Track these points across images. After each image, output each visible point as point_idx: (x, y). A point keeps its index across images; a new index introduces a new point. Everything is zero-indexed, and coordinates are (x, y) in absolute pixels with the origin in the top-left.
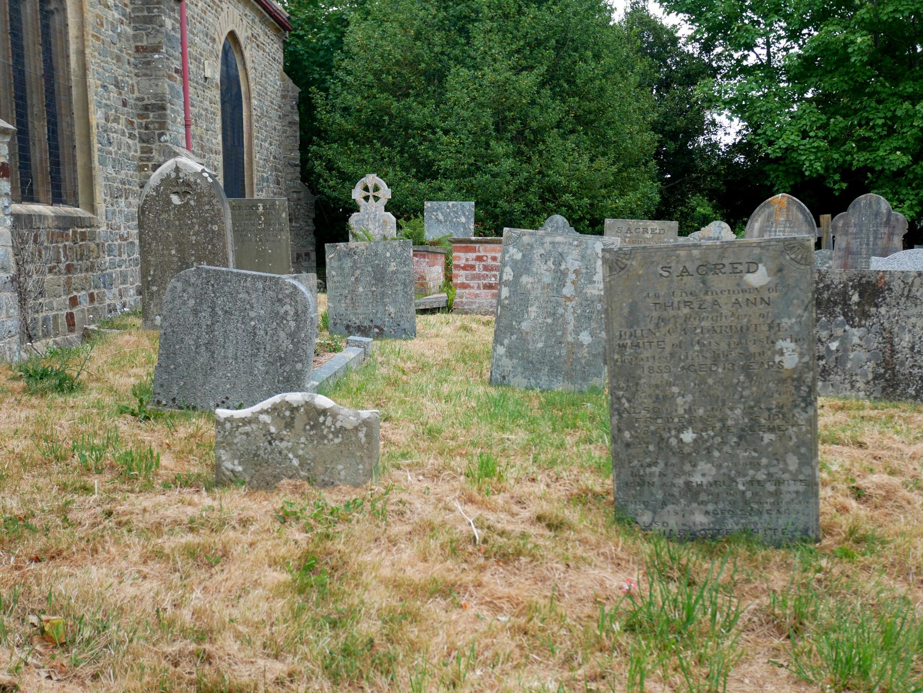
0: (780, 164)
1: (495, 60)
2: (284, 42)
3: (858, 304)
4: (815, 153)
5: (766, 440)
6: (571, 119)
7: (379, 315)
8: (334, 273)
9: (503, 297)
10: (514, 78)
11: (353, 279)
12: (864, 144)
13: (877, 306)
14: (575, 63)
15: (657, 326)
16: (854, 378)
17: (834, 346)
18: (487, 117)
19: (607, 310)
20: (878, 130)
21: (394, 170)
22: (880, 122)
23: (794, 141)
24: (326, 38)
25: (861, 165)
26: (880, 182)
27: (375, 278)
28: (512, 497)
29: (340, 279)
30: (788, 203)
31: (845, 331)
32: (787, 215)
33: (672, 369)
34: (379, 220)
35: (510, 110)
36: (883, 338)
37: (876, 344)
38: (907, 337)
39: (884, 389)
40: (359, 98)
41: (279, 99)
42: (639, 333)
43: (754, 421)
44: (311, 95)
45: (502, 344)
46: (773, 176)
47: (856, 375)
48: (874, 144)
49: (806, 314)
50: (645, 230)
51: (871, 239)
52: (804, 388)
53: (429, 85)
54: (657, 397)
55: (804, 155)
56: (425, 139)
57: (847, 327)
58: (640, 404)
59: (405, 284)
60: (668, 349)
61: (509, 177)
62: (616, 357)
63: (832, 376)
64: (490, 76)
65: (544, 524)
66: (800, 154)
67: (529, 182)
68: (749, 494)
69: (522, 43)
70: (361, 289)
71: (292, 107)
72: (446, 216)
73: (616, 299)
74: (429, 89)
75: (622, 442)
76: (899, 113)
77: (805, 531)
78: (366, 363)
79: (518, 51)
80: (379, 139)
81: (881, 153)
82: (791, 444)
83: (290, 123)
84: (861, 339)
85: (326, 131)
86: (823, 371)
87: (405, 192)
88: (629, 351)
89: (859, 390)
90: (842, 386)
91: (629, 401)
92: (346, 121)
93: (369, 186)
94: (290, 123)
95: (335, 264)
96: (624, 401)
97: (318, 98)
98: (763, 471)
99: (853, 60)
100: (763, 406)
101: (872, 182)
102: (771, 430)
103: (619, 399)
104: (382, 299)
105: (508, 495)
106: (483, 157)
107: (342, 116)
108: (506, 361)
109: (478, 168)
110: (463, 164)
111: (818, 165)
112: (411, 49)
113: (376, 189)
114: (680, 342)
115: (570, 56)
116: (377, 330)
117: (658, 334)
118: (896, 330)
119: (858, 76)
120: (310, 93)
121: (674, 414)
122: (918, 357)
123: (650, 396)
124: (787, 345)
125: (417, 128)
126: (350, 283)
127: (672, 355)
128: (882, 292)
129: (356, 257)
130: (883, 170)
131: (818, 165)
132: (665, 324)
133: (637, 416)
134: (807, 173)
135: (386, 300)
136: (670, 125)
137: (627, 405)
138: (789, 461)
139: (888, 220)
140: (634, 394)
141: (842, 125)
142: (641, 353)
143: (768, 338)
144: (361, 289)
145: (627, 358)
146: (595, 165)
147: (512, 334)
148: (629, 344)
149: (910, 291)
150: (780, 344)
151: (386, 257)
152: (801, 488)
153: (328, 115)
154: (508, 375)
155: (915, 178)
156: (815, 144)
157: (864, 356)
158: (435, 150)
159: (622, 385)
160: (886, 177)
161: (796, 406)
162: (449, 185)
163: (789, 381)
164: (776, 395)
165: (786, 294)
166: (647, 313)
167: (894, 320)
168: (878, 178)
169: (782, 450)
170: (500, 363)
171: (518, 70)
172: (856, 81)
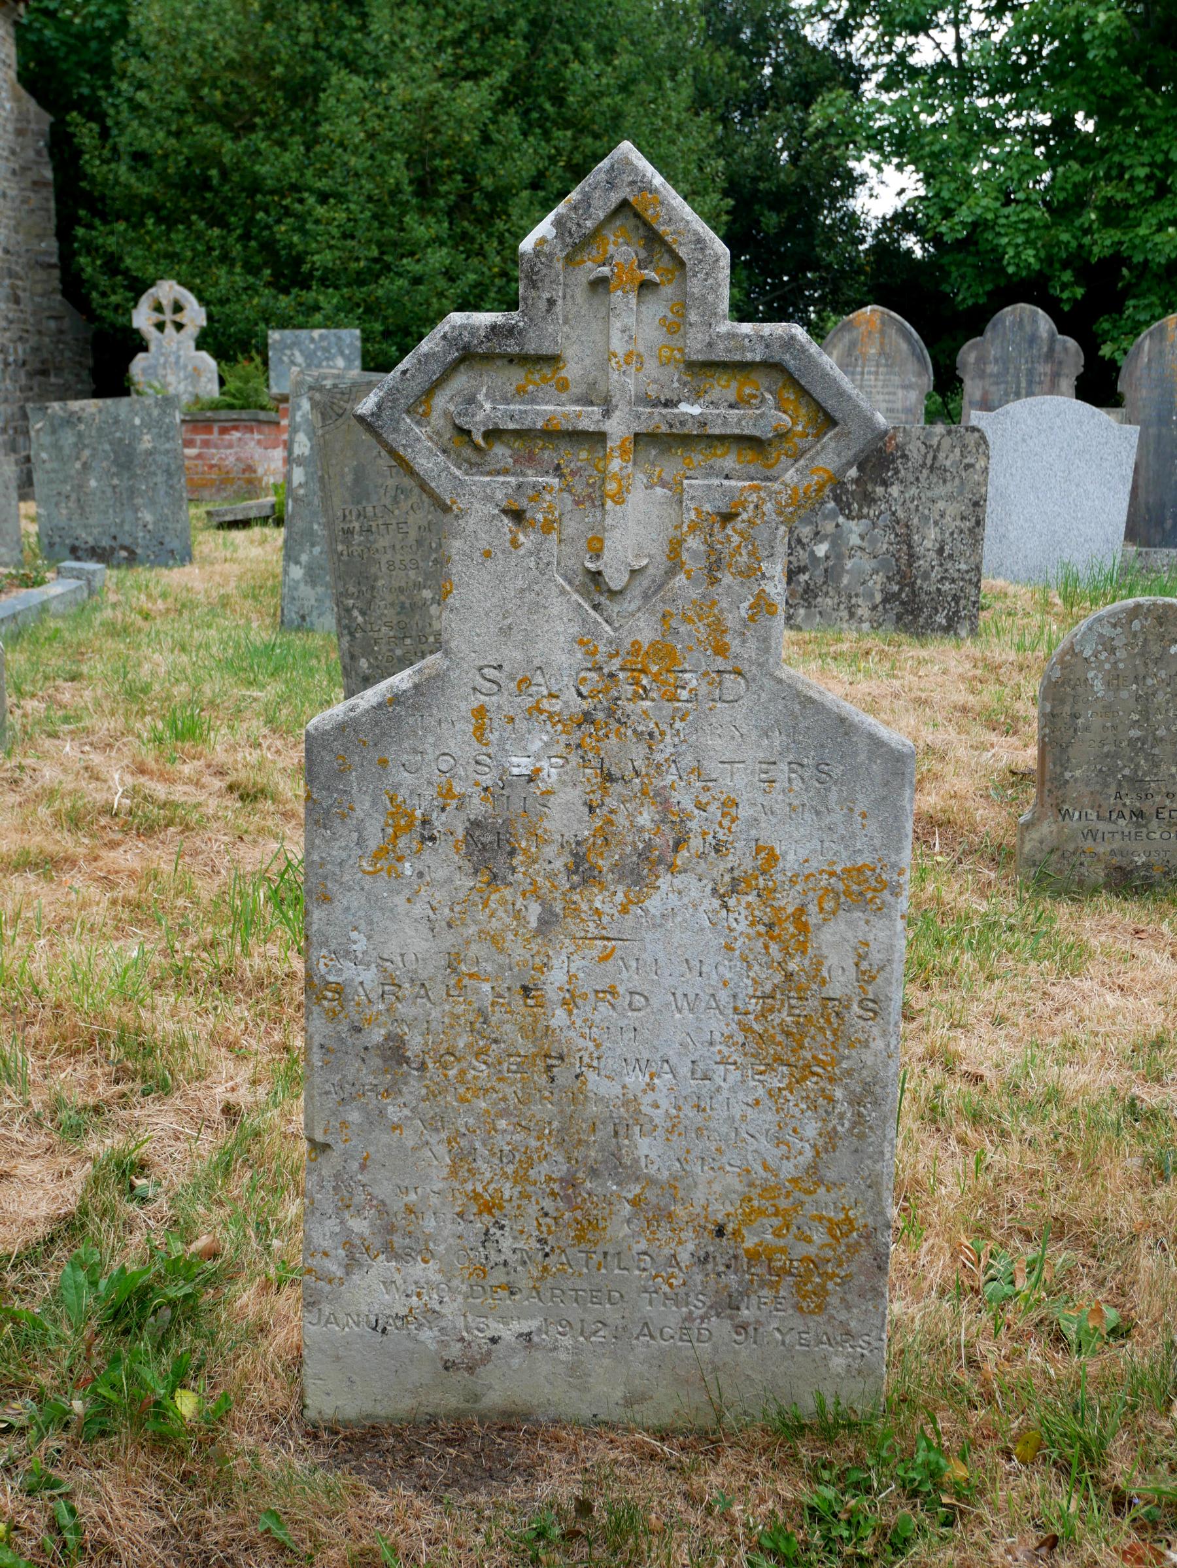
0: (969, 253)
1: (412, 59)
2: (16, 24)
3: (857, 481)
4: (1025, 232)
6: (559, 171)
7: (127, 527)
8: (44, 455)
9: (295, 483)
10: (446, 94)
11: (78, 465)
12: (1113, 214)
13: (885, 484)
14: (565, 63)
15: (395, 500)
16: (853, 601)
17: (821, 550)
18: (398, 171)
19: (321, 478)
20: (1140, 187)
21: (230, 272)
22: (1142, 172)
23: (987, 209)
24: (100, 15)
25: (1107, 252)
26: (1144, 285)
27: (115, 462)
28: (209, 766)
29: (55, 465)
30: (883, 323)
31: (837, 525)
32: (882, 344)
33: (421, 564)
34: (185, 367)
35: (443, 155)
36: (897, 535)
37: (885, 546)
38: (932, 533)
39: (899, 618)
40: (161, 135)
41: (11, 137)
42: (369, 510)
44: (71, 129)
45: (297, 563)
46: (955, 274)
47: (857, 595)
48: (1132, 214)
51: (1024, 384)
53: (291, 109)
54: (403, 607)
55: (1006, 235)
56: (287, 212)
57: (841, 519)
58: (380, 618)
59: (169, 474)
60: (413, 534)
61: (441, 283)
62: (340, 548)
63: (819, 599)
64: (403, 92)
65: (236, 795)
66: (999, 234)
69: (462, 26)
70: (93, 483)
71: (38, 153)
73: (334, 462)
74: (293, 115)
75: (357, 674)
78: (83, 607)
79: (458, 42)
80: (202, 215)
81: (1142, 231)
83: (35, 183)
84: (862, 537)
85: (103, 198)
86: (805, 592)
87: (252, 315)
88: (357, 538)
89: (861, 621)
90: (835, 614)
91: (363, 614)
92: (139, 179)
93: (164, 302)
94: (35, 183)
95: (46, 439)
96: (356, 613)
97: (86, 134)
99: (1091, 55)
101: (1129, 285)
103: (348, 611)
104: (131, 497)
105: (202, 762)
106: (395, 244)
107: (133, 169)
108: (305, 591)
109: (388, 268)
110: (357, 259)
111: (1029, 255)
112: (255, 38)
113: (178, 308)
114: (429, 523)
115: (556, 52)
116: (124, 554)
117: (397, 512)
118: (916, 521)
119: (1106, 86)
120: (69, 125)
121: (428, 630)
122: (949, 565)
123: (392, 604)
125: (272, 192)
126: (73, 472)
127: (419, 542)
128: (893, 461)
129: (82, 427)
130: (1146, 261)
131: (1029, 255)
132: (407, 497)
133: (376, 635)
134: (1011, 270)
135: (139, 501)
136: (768, 179)
137: (360, 619)
139: (1051, 350)
140: (369, 603)
141: (1077, 179)
142: (375, 541)
144: (93, 483)
145: (356, 550)
147: (313, 545)
148: (357, 529)
149: (935, 458)
151: (133, 426)
153: (105, 168)
154: (310, 614)
156: (1026, 216)
157: (868, 565)
158: (304, 232)
159: (352, 589)
160: (1155, 275)
162: (329, 300)
166: (380, 481)
167: (912, 506)
168: (1140, 277)
170: (296, 594)
171: (452, 76)
172: (1103, 97)
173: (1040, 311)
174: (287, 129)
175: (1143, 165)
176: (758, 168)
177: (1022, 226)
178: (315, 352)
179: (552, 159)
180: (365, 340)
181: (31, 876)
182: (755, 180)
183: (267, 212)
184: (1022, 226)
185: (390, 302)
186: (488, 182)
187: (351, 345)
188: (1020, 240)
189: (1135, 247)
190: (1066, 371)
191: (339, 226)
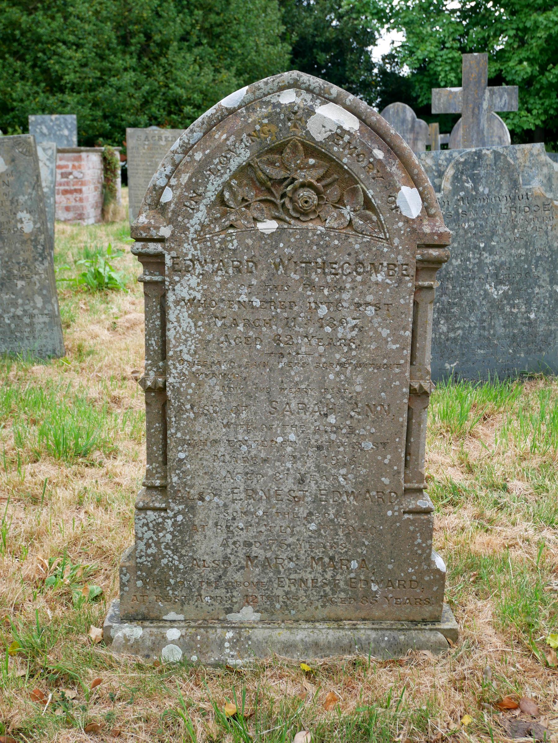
0: (425, 75)
4: (450, 64)
5: (19, 286)
18: (109, 32)
23: (430, 52)
43: (10, 272)
46: (417, 87)
48: (507, 55)
49: (34, 192)
50: (160, 138)
52: (39, 247)
61: (132, 91)
66: (437, 65)
67: (153, 92)
68: (13, 326)
72: (50, 129)
76: (528, 24)
77: (54, 351)
81: (511, 64)
82: (36, 287)
98: (20, 308)
100: (14, 261)
102: (22, 278)
124: (23, 215)
125: (47, 43)
136: (321, 36)
138: (36, 301)
139: (413, 126)
143: (11, 210)
146: (219, 77)
150: (20, 215)
152: (47, 319)
155: (542, 88)
156: (450, 56)
161: (36, 260)
163: (29, 242)
164: (22, 253)
165: (19, 178)
169: (30, 293)
173: (407, 106)
174: (55, 10)
175: (513, 29)
176: (316, 30)
177: (449, 61)
178: (53, 126)
179: (193, 26)
180: (79, 120)
181: (171, 660)
182: (313, 36)
183: (45, 54)
184: (449, 61)
185: (106, 100)
186: (157, 38)
187: (72, 123)
188: (447, 68)
189: (507, 72)
190: (420, 137)
191: (78, 61)
